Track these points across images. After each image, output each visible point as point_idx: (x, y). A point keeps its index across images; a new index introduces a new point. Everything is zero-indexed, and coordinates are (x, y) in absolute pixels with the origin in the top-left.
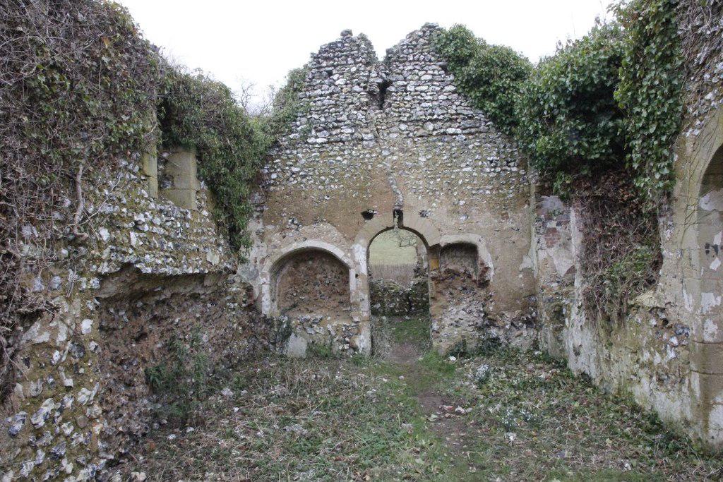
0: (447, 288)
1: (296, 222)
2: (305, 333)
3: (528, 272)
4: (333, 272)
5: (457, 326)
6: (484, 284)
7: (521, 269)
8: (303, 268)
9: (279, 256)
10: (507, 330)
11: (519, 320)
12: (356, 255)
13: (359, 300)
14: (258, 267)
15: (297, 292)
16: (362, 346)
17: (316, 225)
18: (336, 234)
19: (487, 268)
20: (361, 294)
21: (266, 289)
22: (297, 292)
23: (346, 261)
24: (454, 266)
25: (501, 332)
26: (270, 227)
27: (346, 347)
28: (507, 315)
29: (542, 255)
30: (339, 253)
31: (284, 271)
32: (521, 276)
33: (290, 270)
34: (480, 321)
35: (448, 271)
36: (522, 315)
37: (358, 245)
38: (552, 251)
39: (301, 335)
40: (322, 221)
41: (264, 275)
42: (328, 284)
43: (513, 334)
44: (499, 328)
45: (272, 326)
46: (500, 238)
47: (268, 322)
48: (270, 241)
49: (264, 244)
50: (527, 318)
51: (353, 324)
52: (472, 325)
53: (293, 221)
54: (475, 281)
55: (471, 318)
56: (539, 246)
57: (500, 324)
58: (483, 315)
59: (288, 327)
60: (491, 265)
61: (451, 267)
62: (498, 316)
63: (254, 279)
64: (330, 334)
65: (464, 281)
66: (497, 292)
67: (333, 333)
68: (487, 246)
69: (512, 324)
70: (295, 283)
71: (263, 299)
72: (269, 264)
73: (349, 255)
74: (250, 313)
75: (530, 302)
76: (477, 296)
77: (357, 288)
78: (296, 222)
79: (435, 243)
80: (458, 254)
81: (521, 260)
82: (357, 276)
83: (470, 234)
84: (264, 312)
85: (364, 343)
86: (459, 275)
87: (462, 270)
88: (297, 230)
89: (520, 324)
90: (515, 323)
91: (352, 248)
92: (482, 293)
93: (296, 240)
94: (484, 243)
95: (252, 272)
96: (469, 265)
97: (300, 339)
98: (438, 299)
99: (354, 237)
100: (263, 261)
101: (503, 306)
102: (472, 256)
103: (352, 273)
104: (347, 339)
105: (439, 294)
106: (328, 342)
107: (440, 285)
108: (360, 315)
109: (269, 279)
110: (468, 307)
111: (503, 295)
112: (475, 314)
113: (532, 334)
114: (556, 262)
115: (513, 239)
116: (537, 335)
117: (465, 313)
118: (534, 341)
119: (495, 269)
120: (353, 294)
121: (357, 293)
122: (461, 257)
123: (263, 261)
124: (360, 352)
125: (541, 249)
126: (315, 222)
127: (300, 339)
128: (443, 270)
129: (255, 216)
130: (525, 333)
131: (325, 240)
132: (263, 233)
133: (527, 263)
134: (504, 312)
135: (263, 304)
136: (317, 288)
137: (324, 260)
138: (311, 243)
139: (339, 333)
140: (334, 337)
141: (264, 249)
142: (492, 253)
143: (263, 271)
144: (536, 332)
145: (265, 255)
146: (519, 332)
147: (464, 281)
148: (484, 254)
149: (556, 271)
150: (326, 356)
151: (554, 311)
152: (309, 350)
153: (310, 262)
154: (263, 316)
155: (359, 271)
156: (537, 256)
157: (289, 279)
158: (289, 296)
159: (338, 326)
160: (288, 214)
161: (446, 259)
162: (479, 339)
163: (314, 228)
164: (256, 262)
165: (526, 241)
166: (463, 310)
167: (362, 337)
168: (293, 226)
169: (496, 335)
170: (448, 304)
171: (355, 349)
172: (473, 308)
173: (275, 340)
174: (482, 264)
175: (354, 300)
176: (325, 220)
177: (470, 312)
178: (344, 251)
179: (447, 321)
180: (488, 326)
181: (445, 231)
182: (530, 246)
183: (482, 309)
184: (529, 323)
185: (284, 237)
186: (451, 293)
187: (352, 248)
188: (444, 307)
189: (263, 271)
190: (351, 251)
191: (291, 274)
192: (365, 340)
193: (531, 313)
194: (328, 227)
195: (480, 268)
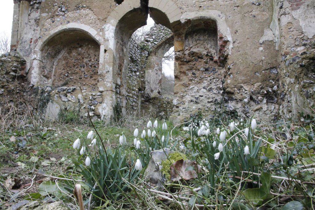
0: (191, 69)
1: (63, 10)
2: (60, 100)
3: (269, 44)
4: (96, 56)
5: (197, 103)
6: (223, 61)
7: (261, 41)
8: (74, 54)
9: (47, 37)
10: (245, 103)
11: (259, 93)
12: (106, 33)
13: (105, 72)
14: (32, 46)
15: (68, 73)
16: (104, 114)
17: (78, 11)
18: (92, 16)
19: (226, 42)
20: (107, 66)
21: (36, 63)
22: (68, 73)
23: (97, 38)
24: (198, 49)
25: (239, 105)
26: (44, 15)
27: (91, 114)
28: (246, 87)
29: (285, 20)
30: (93, 32)
31: (60, 56)
32: (261, 49)
33: (65, 55)
34: (219, 98)
35: (193, 54)
36: (262, 88)
37: (108, 25)
38: (296, 14)
39: (57, 103)
40: (83, 7)
41: (35, 52)
42: (91, 66)
43: (252, 107)
44: (237, 101)
45: (37, 94)
46: (240, 12)
47: (34, 90)
48: (43, 25)
49: (39, 28)
50: (268, 91)
51: (99, 94)
52: (211, 102)
53: (61, 9)
54: (216, 62)
55: (211, 95)
56: (282, 11)
57: (238, 96)
58: (222, 92)
59: (49, 95)
60: (229, 38)
61: (195, 50)
62: (236, 89)
63: (28, 56)
64: (79, 102)
65: (206, 63)
66: (235, 64)
67: (82, 101)
68: (226, 20)
69: (251, 98)
70: (67, 65)
71: (33, 72)
72: (40, 43)
73: (101, 33)
74: (23, 84)
75: (272, 75)
76: (217, 74)
77: (104, 61)
78: (63, 10)
79: (176, 19)
80: (202, 38)
81: (262, 33)
82: (105, 51)
83: (210, 11)
84: (32, 83)
85: (106, 111)
86: (202, 58)
87: (205, 52)
88: (63, 16)
89: (260, 98)
90: (254, 97)
91: (103, 27)
92: (223, 71)
93: (61, 24)
94: (224, 18)
95: (27, 50)
96: (211, 47)
97: (56, 106)
98: (181, 78)
99: (106, 18)
100: (37, 41)
101: (241, 78)
102: (215, 39)
103: (102, 48)
104: (92, 107)
105: (182, 75)
106: (77, 109)
107: (184, 67)
108: (105, 86)
109: (39, 56)
110: (208, 85)
111: (241, 68)
112: (215, 91)
113: (273, 108)
114: (302, 24)
115: (253, 13)
116: (279, 109)
117: (205, 90)
118: (275, 116)
119: (234, 42)
120: (100, 67)
121: (104, 66)
122: (204, 40)
123: (37, 41)
124: (102, 119)
125: (285, 14)
126: (78, 8)
127: (56, 106)
128: (187, 52)
129: (35, 7)
130: (265, 107)
131: (83, 23)
132: (39, 19)
133: (268, 35)
134: (242, 85)
135: (32, 75)
136: (83, 69)
137: (90, 46)
138: (73, 25)
139: (86, 102)
140: (82, 105)
141: (38, 32)
142: (231, 27)
143: (35, 49)
144: (277, 106)
145: (38, 36)
146: (259, 106)
147: (206, 63)
148: (224, 29)
149: (302, 33)
150: (72, 120)
151: (301, 66)
152: (61, 115)
153: (80, 49)
154: (31, 85)
155: (107, 47)
156: (279, 24)
157: (64, 62)
158: (62, 76)
159: (86, 96)
160: (58, 4)
161: (190, 42)
162: (215, 112)
163: (77, 14)
164: (31, 42)
165: (267, 15)
166: (204, 88)
167: (104, 105)
168: (61, 13)
169: (234, 108)
170: (190, 82)
171: (99, 116)
172: (213, 86)
173: (37, 106)
174: (221, 38)
175: (101, 72)
176: (85, 6)
177: (210, 90)
178: (97, 30)
179: (188, 98)
180: (226, 101)
181: (185, 9)
182: (272, 18)
183: (221, 86)
184: (270, 97)
185: (53, 22)
186: (193, 74)
187: (103, 27)
188: (186, 86)
189: (35, 49)
190: (102, 30)
191: (65, 58)
192: (107, 108)
193: (272, 87)
194: (87, 11)
195: (220, 43)
